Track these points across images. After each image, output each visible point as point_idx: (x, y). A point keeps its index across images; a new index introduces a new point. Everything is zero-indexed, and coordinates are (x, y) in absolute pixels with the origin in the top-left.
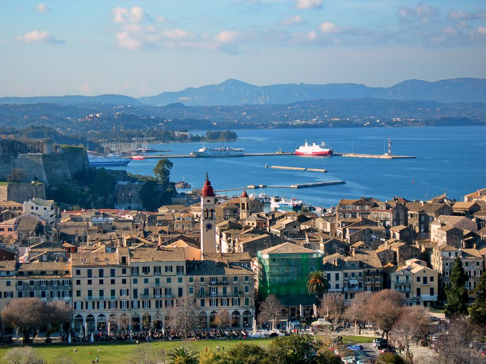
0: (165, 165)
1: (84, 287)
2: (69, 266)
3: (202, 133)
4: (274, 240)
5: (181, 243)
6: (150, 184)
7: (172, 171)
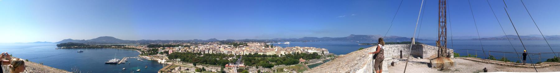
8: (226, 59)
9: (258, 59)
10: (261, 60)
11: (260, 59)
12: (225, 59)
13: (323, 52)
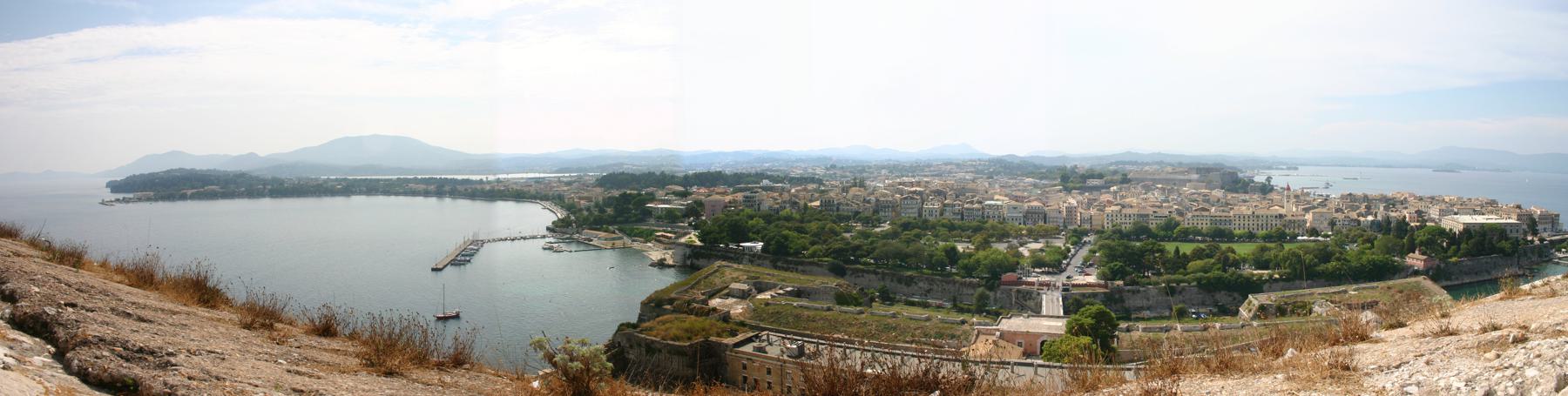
0: (1269, 179)
1: (1237, 222)
2: (1232, 213)
3: (1284, 167)
4: (1314, 208)
5: (1277, 207)
6: (1264, 185)
7: (1272, 181)
8: (1011, 247)
9: (1177, 251)
10: (1198, 254)
11: (1188, 252)
12: (1002, 247)
13: (954, 366)
